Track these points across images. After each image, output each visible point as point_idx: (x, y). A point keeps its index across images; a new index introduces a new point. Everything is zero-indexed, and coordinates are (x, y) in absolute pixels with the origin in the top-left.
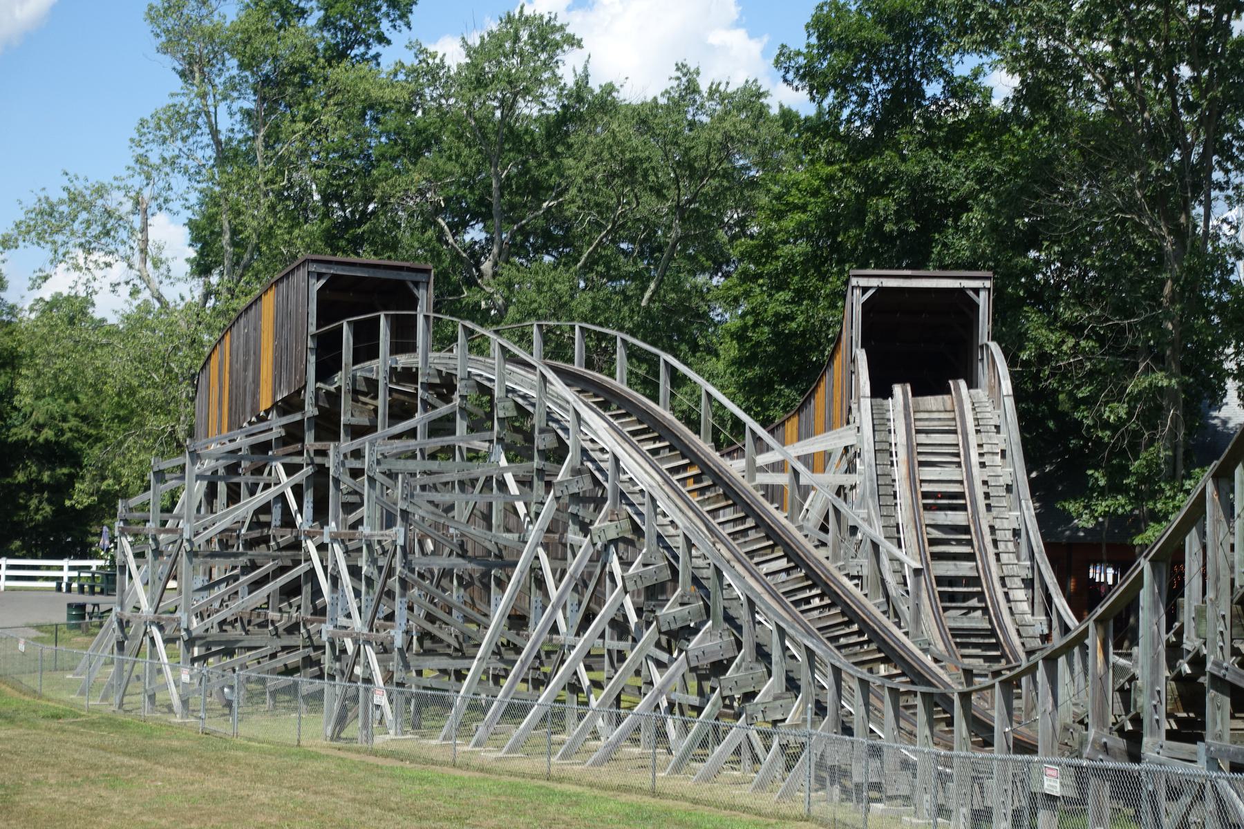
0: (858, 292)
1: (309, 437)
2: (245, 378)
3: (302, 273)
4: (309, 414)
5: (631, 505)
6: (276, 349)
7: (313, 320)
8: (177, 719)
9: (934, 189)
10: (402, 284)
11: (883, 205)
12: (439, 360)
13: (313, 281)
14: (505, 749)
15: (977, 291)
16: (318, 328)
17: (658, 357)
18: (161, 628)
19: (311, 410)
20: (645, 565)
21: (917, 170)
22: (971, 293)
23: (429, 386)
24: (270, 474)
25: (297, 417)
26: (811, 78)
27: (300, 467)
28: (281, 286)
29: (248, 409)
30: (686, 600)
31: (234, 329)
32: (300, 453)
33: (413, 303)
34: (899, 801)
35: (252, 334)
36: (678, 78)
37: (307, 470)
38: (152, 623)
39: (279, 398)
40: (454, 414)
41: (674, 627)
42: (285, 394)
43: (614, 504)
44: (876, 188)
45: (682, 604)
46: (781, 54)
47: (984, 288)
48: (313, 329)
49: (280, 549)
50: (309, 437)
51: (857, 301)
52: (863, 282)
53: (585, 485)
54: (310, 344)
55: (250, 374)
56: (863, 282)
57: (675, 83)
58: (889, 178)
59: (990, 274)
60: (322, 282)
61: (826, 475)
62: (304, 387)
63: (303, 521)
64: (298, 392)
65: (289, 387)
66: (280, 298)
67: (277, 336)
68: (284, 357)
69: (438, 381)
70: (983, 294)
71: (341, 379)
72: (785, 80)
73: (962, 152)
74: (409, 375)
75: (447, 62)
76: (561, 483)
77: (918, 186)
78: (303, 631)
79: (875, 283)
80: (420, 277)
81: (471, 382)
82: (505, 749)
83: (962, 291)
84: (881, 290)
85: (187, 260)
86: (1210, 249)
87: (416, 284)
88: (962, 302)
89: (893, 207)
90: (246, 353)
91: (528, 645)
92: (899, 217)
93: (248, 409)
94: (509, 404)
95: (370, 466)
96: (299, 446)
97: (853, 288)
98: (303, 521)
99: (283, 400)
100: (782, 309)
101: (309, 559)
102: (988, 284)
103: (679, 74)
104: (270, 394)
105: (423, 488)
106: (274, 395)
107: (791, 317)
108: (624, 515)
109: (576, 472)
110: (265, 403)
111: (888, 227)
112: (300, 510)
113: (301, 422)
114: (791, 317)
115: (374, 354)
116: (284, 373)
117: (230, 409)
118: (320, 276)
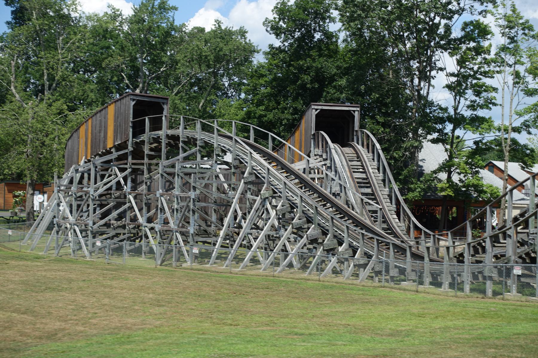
0: (314, 110)
1: (130, 158)
2: (100, 136)
3: (128, 99)
4: (130, 150)
5: (272, 185)
6: (115, 126)
7: (131, 116)
8: (88, 259)
9: (324, 72)
10: (159, 103)
11: (306, 78)
12: (189, 133)
13: (131, 102)
14: (240, 268)
15: (354, 111)
16: (133, 119)
17: (268, 134)
18: (78, 226)
19: (130, 148)
20: (283, 206)
21: (319, 66)
22: (352, 112)
23: (184, 142)
24: (112, 171)
25: (126, 151)
26: (276, 30)
27: (126, 169)
28: (117, 103)
29: (101, 147)
30: (301, 218)
31: (94, 118)
32: (126, 164)
33: (161, 111)
34: (412, 281)
35: (103, 120)
36: (215, 25)
37: (129, 170)
38: (74, 224)
39: (116, 143)
40: (196, 152)
41: (297, 227)
42: (120, 142)
43: (267, 185)
44: (301, 69)
45: (299, 219)
46: (266, 21)
48: (131, 119)
49: (116, 198)
50: (130, 158)
51: (314, 113)
52: (316, 107)
53: (253, 178)
54: (131, 125)
55: (102, 135)
56: (316, 107)
57: (214, 26)
58: (308, 68)
59: (359, 105)
60: (135, 102)
62: (128, 140)
63: (127, 189)
64: (125, 142)
65: (121, 139)
66: (117, 108)
67: (116, 120)
68: (119, 129)
69: (186, 140)
70: (356, 112)
71: (144, 137)
72: (267, 31)
73: (332, 59)
74: (176, 138)
75: (123, 13)
76: (246, 177)
77: (318, 71)
78: (127, 227)
79: (320, 107)
80: (165, 101)
81: (203, 141)
82: (240, 268)
83: (349, 111)
84: (322, 110)
87: (163, 103)
88: (349, 115)
89: (310, 79)
90: (100, 126)
92: (312, 82)
93: (101, 147)
94: (219, 149)
95: (178, 171)
96: (126, 161)
98: (127, 189)
99: (118, 145)
100: (262, 113)
101: (130, 202)
102: (358, 109)
103: (216, 23)
104: (112, 142)
105: (199, 178)
106: (114, 142)
107: (265, 116)
108: (271, 189)
109: (250, 174)
110: (110, 145)
111: (308, 86)
112: (126, 184)
113: (127, 153)
114: (265, 116)
115: (160, 129)
116: (118, 135)
117: (92, 147)
118: (134, 100)
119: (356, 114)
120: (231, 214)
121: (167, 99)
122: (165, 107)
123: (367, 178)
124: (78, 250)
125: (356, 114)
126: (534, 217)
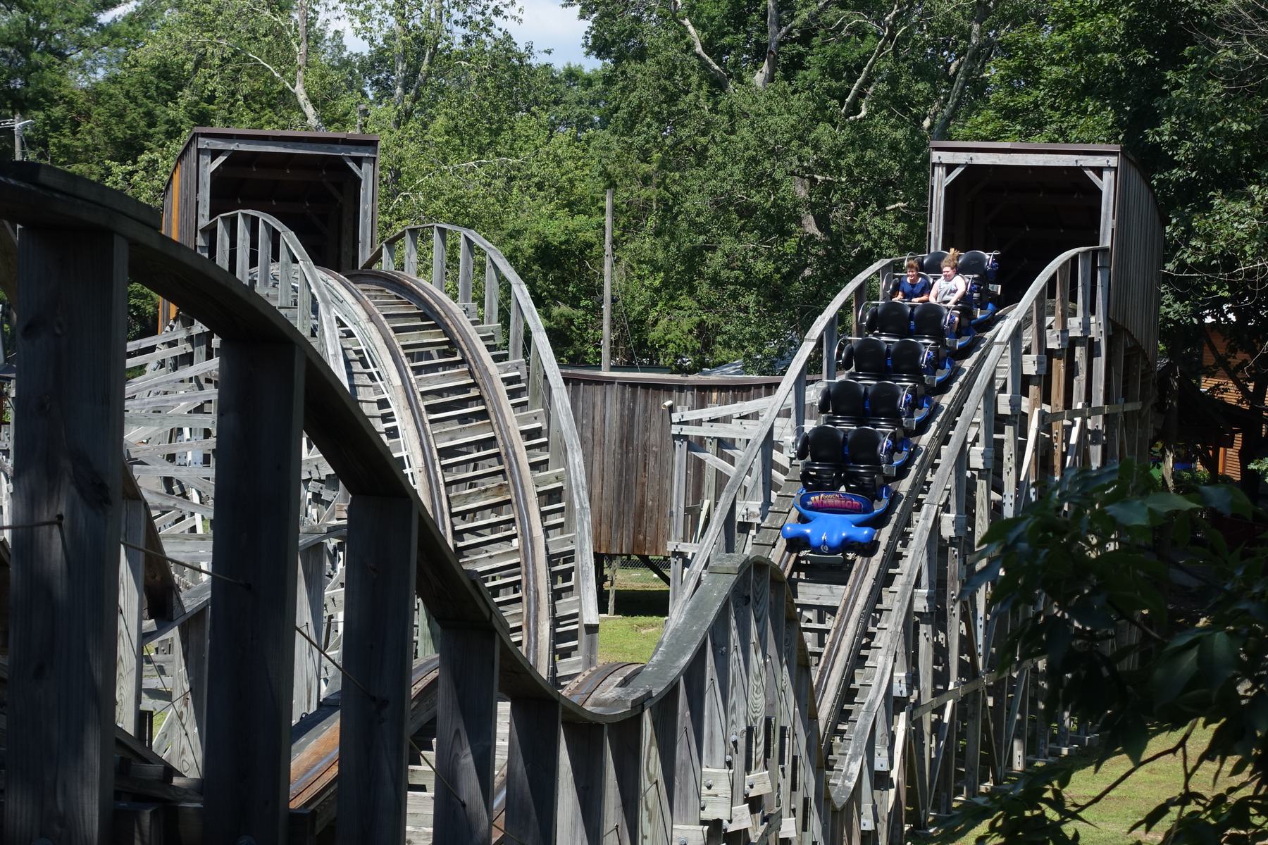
0: (939, 171)
13: (205, 159)
15: (1099, 171)
17: (949, 189)
22: (1090, 174)
47: (1109, 168)
51: (940, 182)
52: (948, 158)
56: (948, 158)
59: (1117, 148)
61: (494, 364)
70: (1108, 176)
79: (962, 158)
83: (1078, 171)
84: (971, 169)
85: (569, 64)
86: (1037, 592)
87: (358, 161)
91: (413, 381)
97: (934, 165)
102: (1113, 161)
119: (1106, 184)
120: (663, 496)
121: (373, 144)
122: (365, 173)
123: (452, 343)
124: (612, 557)
125: (1106, 184)
126: (472, 515)
